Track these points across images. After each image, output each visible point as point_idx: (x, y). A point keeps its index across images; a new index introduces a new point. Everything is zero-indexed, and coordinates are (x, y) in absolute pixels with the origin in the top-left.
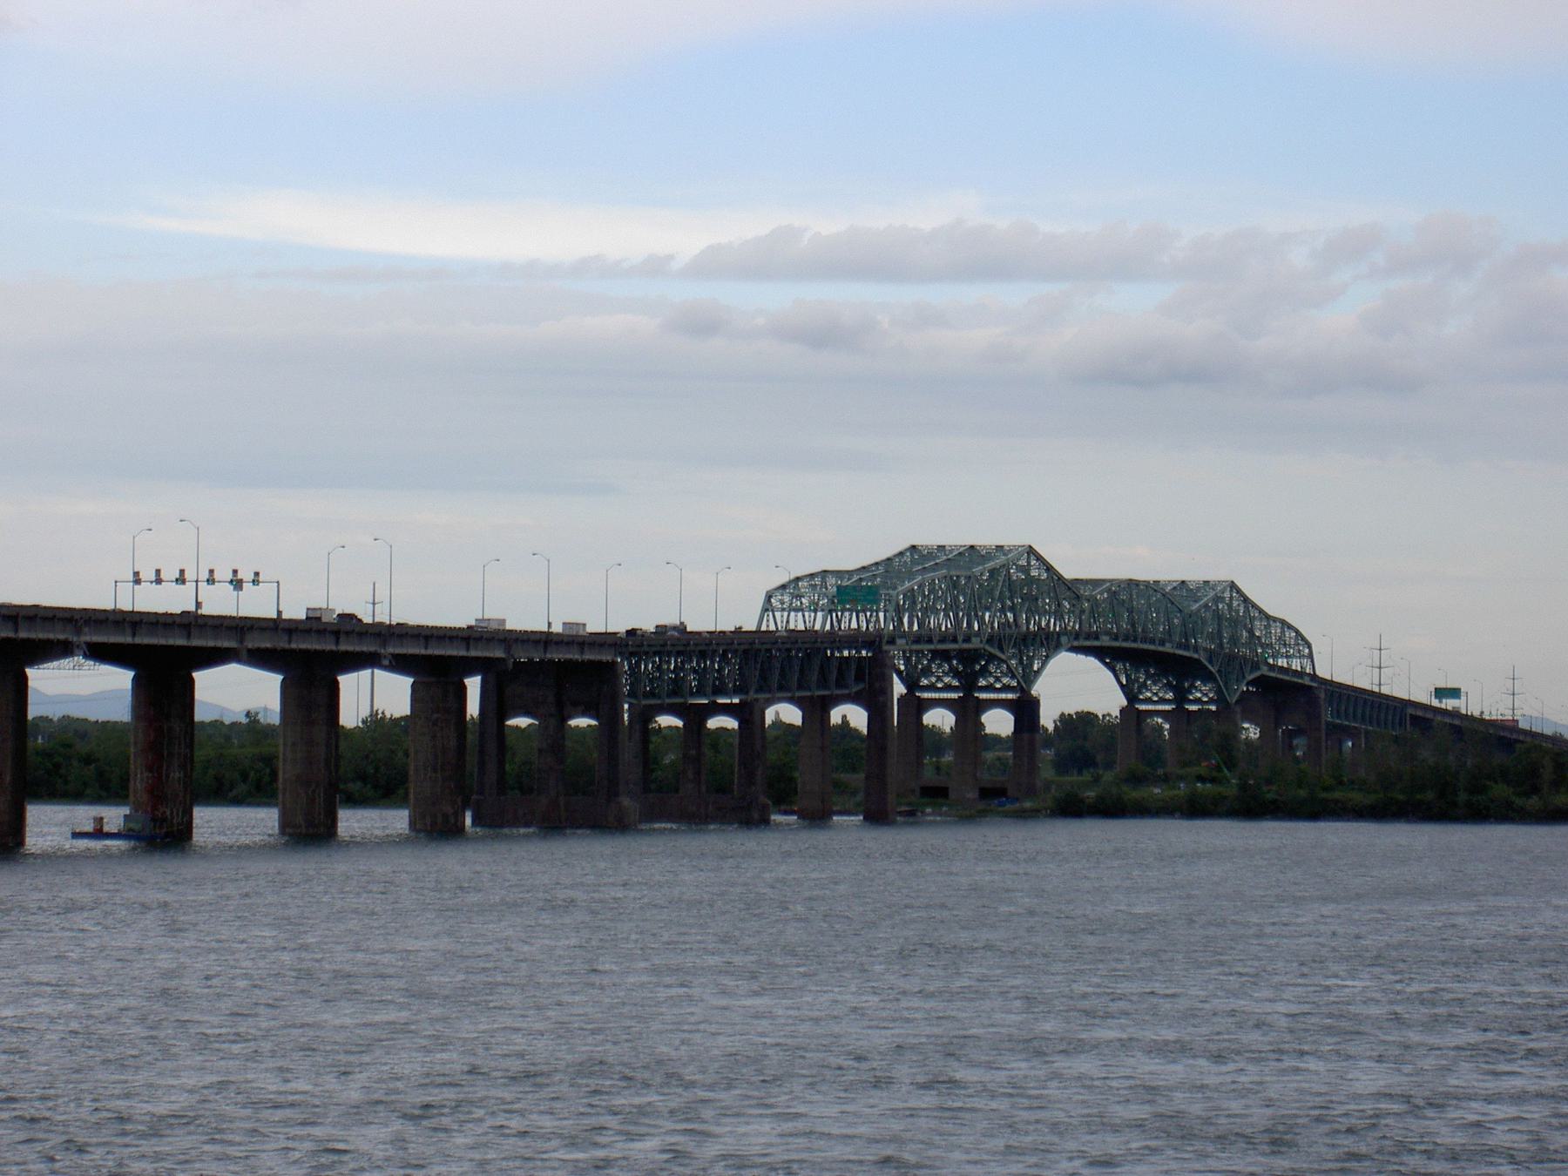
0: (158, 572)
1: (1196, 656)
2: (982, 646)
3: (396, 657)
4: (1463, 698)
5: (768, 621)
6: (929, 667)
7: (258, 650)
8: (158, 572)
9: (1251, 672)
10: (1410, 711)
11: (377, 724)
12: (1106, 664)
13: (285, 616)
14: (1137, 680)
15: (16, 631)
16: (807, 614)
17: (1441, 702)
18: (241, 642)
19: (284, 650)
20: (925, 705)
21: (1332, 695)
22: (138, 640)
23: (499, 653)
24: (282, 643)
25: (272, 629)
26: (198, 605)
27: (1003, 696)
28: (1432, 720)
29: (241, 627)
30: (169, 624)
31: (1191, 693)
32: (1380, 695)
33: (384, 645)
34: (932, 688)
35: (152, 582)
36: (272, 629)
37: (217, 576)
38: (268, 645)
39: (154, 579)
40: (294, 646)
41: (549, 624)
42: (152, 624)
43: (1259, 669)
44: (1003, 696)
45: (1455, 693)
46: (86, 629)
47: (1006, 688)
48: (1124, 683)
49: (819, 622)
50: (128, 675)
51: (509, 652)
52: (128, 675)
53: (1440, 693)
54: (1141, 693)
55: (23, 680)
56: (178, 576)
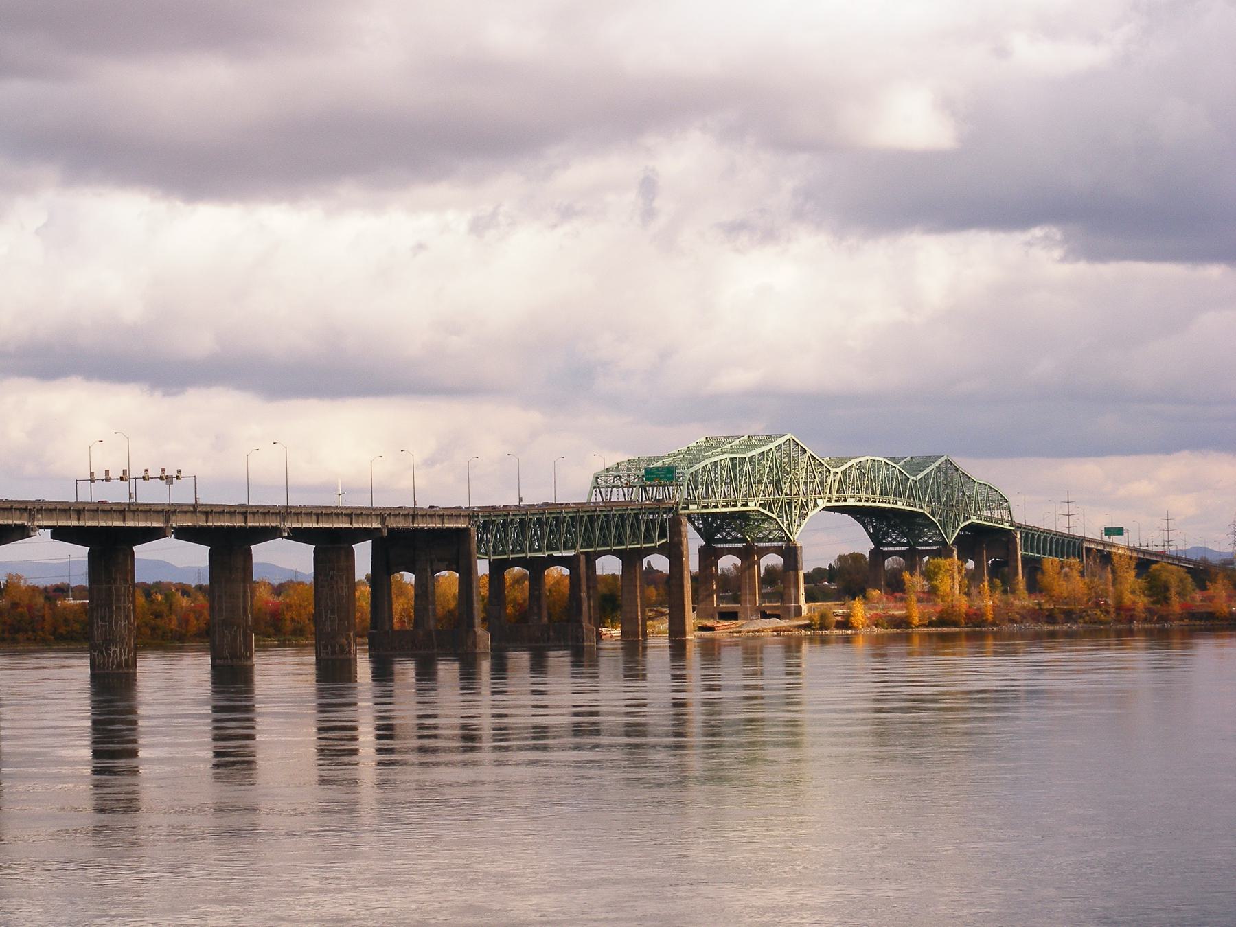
0: (107, 472)
1: (921, 511)
2: (756, 508)
3: (292, 530)
4: (1126, 534)
5: (596, 495)
6: (721, 525)
7: (181, 528)
8: (107, 472)
9: (964, 521)
10: (1086, 544)
11: (558, 582)
12: (857, 519)
13: (200, 502)
14: (880, 529)
15: (246, 522)
16: (625, 489)
17: (1109, 538)
18: (167, 521)
19: (202, 528)
20: (721, 553)
21: (1027, 534)
22: (82, 524)
23: (376, 525)
24: (201, 522)
25: (192, 512)
26: (521, 500)
27: (898, 549)
28: (1103, 551)
29: (168, 511)
30: (232, 512)
31: (921, 538)
32: (1068, 536)
33: (283, 520)
34: (724, 540)
35: (103, 480)
36: (192, 512)
37: (111, 475)
38: (190, 524)
39: (104, 477)
40: (210, 524)
41: (521, 500)
42: (93, 511)
43: (970, 518)
44: (898, 549)
45: (1119, 531)
46: (40, 516)
47: (735, 540)
48: (871, 531)
49: (636, 495)
50: (85, 550)
51: (384, 524)
52: (85, 550)
53: (1109, 532)
54: (884, 539)
55: (249, 554)
56: (143, 475)
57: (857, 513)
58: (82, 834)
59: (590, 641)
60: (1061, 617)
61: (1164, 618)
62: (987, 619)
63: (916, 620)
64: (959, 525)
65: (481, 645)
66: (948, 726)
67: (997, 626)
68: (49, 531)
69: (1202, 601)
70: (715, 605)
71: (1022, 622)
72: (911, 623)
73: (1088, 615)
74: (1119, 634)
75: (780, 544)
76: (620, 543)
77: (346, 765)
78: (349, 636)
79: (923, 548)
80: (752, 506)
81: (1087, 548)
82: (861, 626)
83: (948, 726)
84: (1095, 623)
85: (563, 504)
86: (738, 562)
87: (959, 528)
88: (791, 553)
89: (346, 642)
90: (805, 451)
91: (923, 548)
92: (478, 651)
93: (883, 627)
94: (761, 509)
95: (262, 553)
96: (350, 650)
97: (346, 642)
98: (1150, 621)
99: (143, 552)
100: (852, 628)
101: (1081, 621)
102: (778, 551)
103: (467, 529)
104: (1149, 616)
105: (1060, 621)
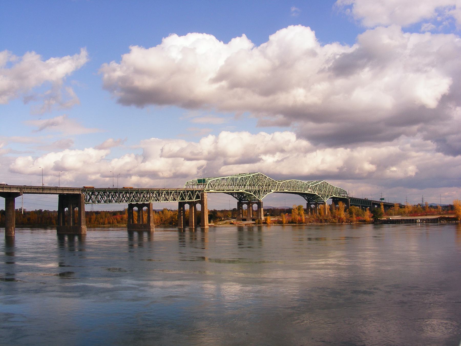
4: (385, 200)
10: (372, 202)
26: (43, 185)
34: (312, 202)
45: (383, 199)
59: (153, 229)
60: (323, 221)
61: (351, 222)
62: (303, 222)
63: (284, 222)
64: (329, 197)
65: (83, 231)
67: (306, 223)
68: (58, 195)
69: (256, 220)
70: (241, 217)
71: (313, 223)
72: (283, 223)
73: (331, 221)
74: (340, 225)
75: (256, 201)
77: (115, 269)
78: (12, 228)
79: (311, 203)
81: (372, 203)
82: (269, 224)
84: (333, 223)
85: (5, 184)
86: (314, 206)
87: (329, 198)
88: (259, 204)
89: (11, 230)
90: (328, 184)
91: (311, 203)
92: (82, 233)
93: (276, 224)
94: (245, 192)
96: (12, 233)
97: (11, 230)
98: (348, 222)
100: (267, 224)
101: (329, 222)
102: (256, 203)
104: (348, 221)
105: (323, 222)
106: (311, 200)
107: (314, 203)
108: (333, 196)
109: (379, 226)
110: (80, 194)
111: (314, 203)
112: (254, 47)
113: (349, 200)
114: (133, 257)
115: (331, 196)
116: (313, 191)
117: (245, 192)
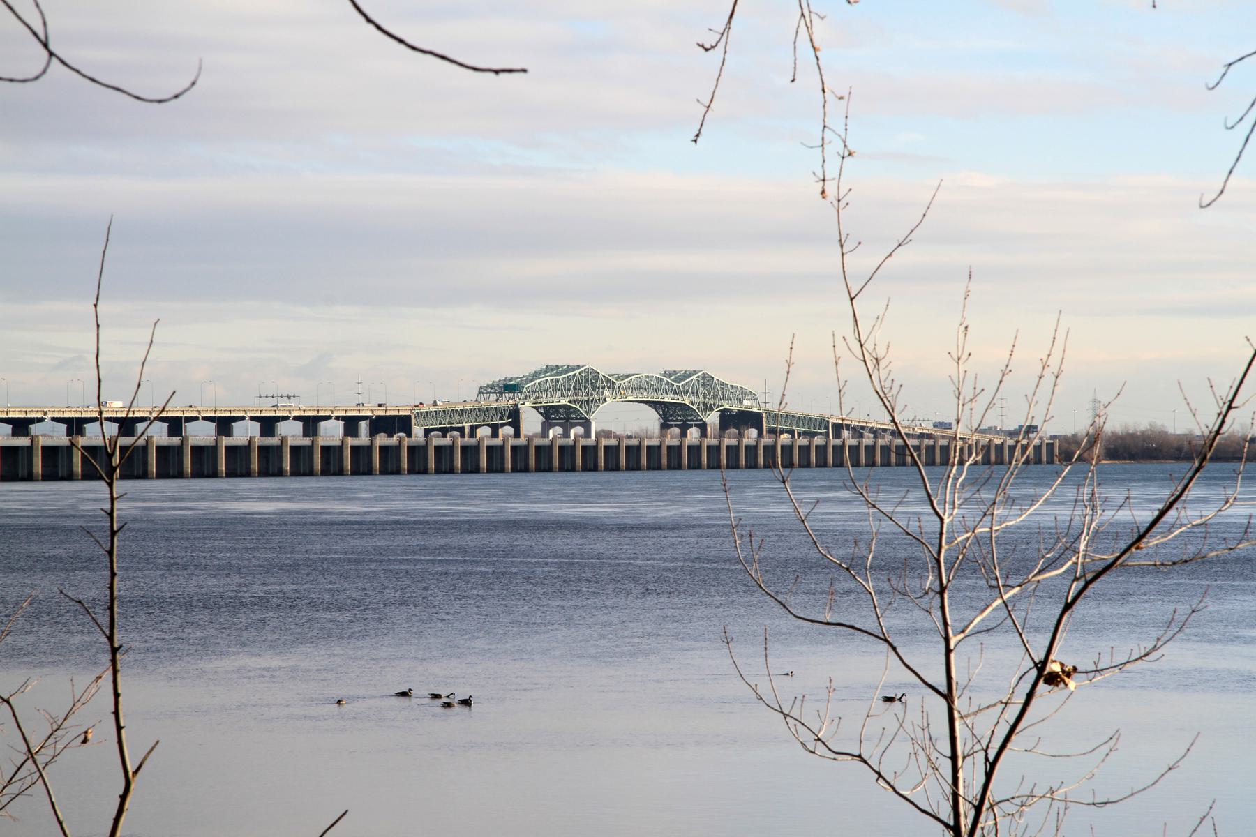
23: (370, 414)
27: (580, 421)
50: (11, 426)
52: (11, 426)
57: (653, 404)
58: (163, 632)
66: (708, 515)
76: (492, 421)
80: (563, 402)
83: (708, 515)
94: (569, 404)
95: (190, 428)
99: (323, 424)
103: (410, 416)
106: (671, 415)
107: (698, 423)
108: (722, 408)
109: (393, 484)
110: (498, 437)
111: (698, 423)
112: (949, 757)
113: (764, 415)
114: (1095, 390)
115: (718, 407)
116: (680, 397)
117: (569, 404)
